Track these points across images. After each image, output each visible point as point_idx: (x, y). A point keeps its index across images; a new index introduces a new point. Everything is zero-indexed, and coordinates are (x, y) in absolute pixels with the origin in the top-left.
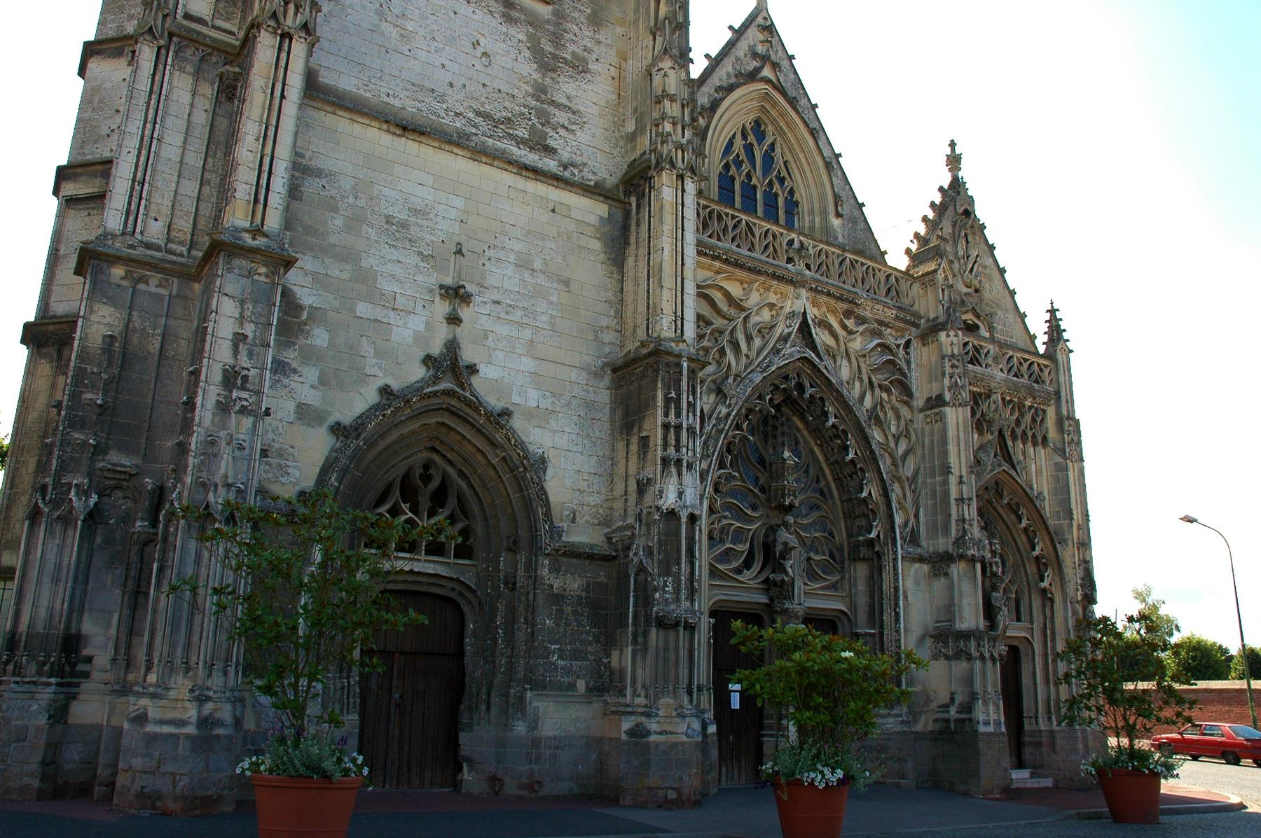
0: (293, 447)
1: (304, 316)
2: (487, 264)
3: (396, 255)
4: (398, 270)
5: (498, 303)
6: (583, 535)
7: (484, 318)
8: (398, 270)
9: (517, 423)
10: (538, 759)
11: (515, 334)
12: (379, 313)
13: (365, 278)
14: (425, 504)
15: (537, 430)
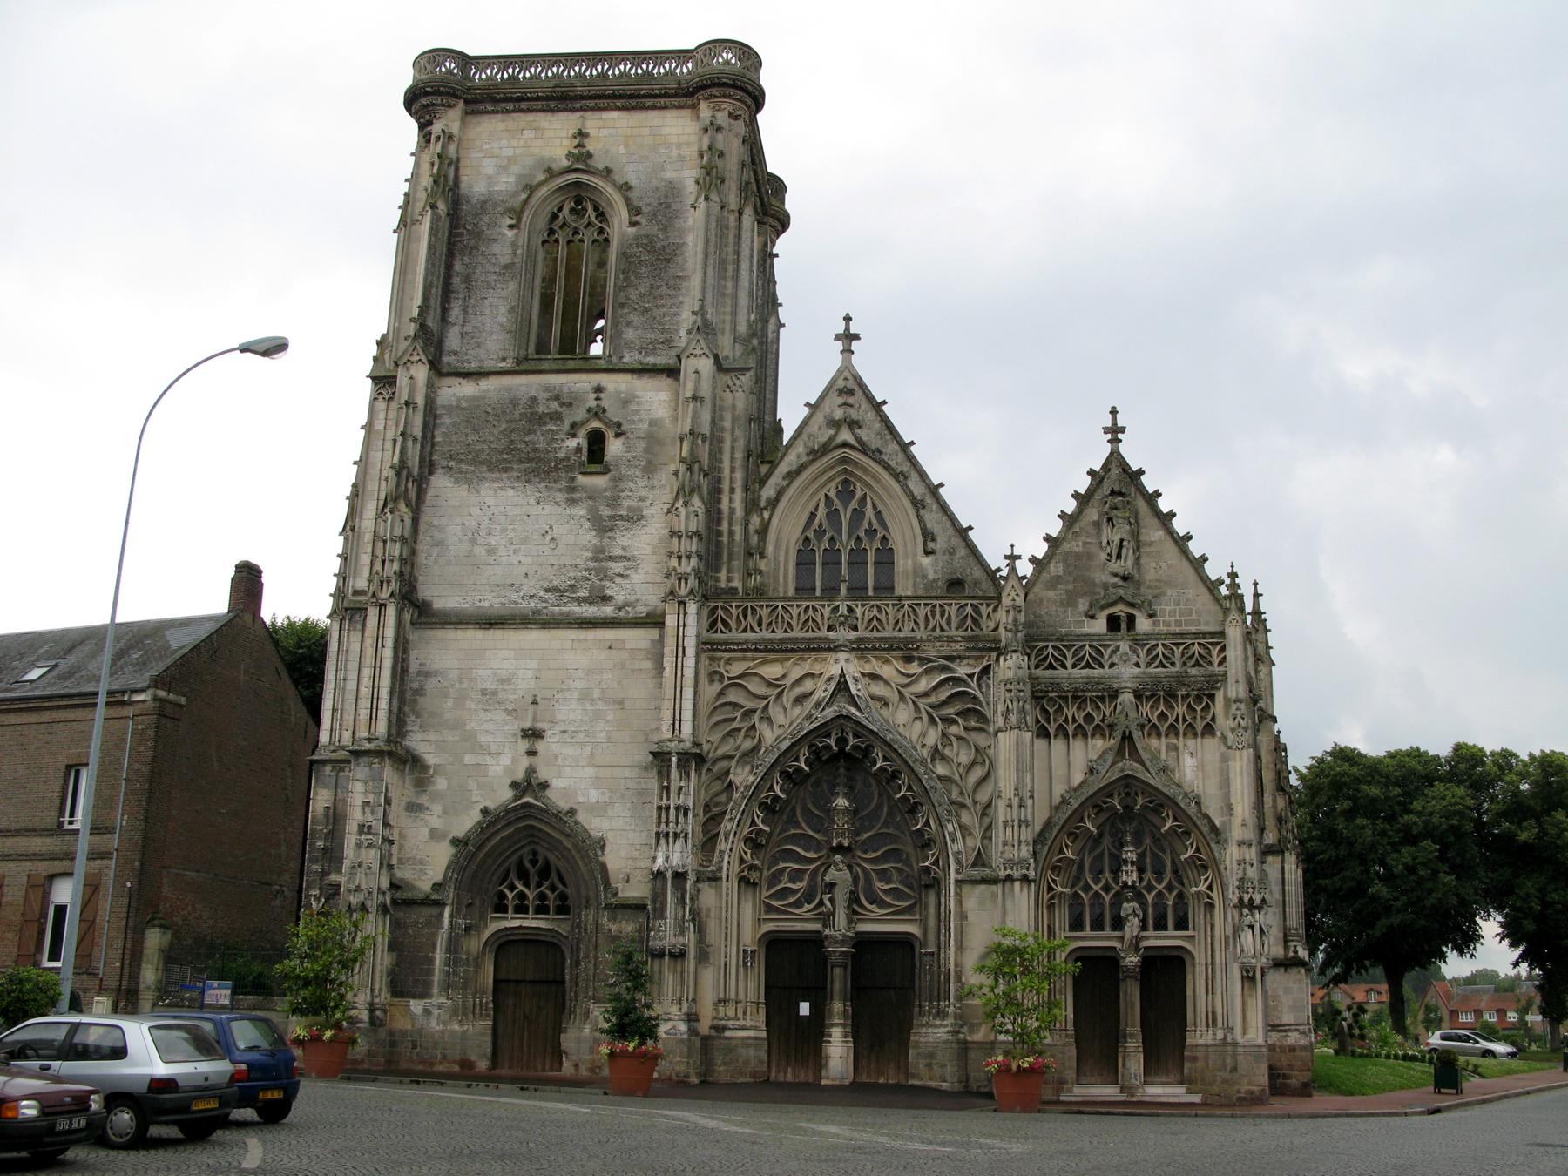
3: (489, 715)
4: (491, 726)
8: (491, 726)
12: (479, 759)
13: (470, 738)
14: (534, 879)
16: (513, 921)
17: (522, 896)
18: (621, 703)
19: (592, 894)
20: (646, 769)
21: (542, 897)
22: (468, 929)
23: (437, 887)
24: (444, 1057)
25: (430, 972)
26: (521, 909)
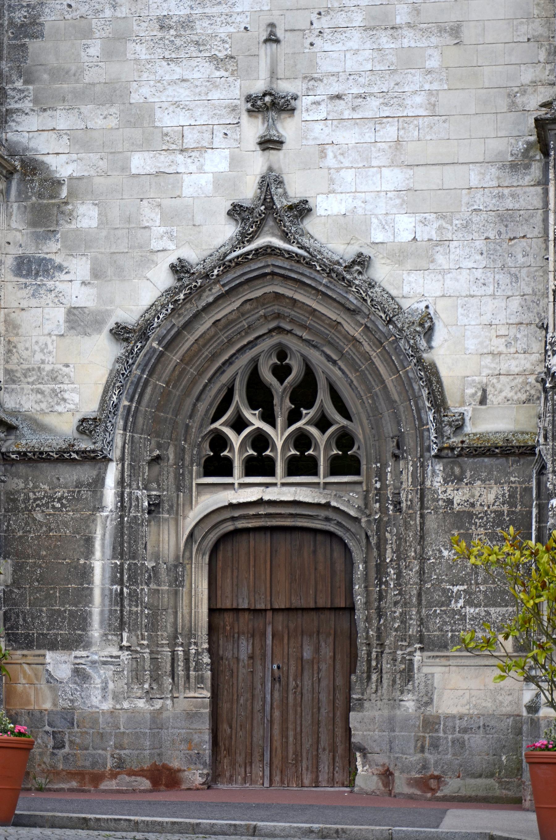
0: (67, 366)
1: (64, 193)
2: (318, 42)
3: (178, 71)
4: (183, 93)
5: (338, 97)
6: (494, 422)
7: (318, 126)
8: (183, 93)
9: (381, 272)
10: (435, 745)
11: (369, 137)
12: (163, 162)
13: (139, 118)
14: (282, 406)
15: (414, 276)
16: (244, 491)
17: (260, 441)
18: (455, 31)
19: (406, 428)
20: (514, 167)
21: (302, 441)
22: (154, 508)
23: (87, 427)
24: (120, 763)
25: (85, 595)
26: (259, 466)
